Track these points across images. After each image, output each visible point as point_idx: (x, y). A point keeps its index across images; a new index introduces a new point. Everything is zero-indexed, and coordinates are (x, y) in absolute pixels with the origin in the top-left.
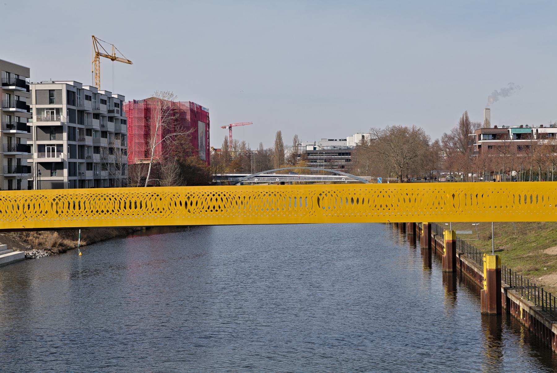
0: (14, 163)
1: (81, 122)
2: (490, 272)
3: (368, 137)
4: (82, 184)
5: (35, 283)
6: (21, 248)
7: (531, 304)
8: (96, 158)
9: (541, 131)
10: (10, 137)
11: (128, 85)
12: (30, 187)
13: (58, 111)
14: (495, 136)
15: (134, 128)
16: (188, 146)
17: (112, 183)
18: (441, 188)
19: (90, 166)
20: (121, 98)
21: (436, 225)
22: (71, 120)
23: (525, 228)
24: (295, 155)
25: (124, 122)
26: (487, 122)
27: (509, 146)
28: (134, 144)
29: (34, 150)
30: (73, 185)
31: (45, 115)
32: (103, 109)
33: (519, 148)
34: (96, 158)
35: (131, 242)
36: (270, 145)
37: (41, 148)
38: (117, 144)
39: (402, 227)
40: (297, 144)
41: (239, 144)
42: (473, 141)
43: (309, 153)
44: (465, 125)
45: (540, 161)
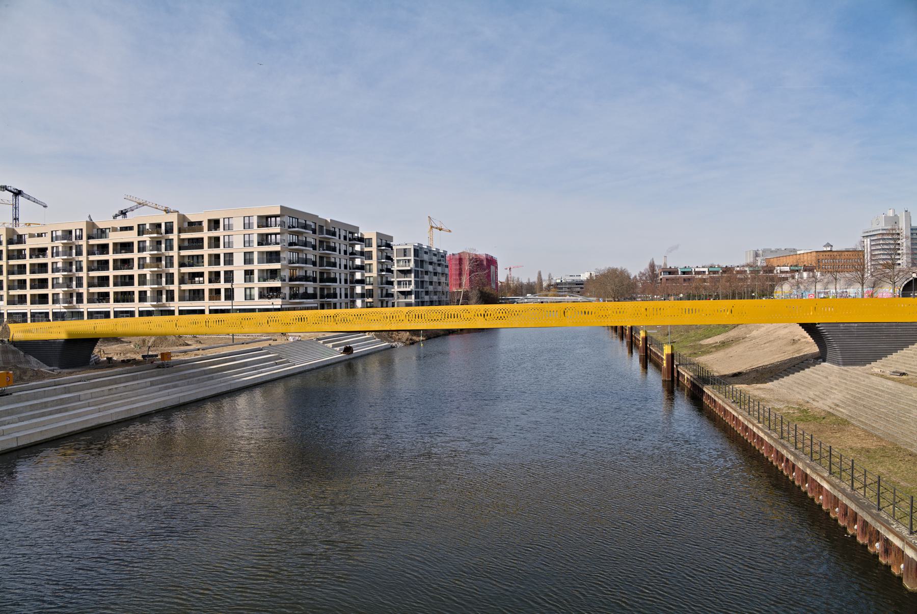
0: (384, 292)
1: (422, 267)
2: (667, 355)
3: (594, 274)
4: (423, 304)
5: (397, 360)
6: (389, 341)
7: (692, 374)
8: (431, 288)
9: (697, 270)
10: (382, 276)
11: (449, 245)
12: (393, 306)
13: (409, 261)
14: (670, 273)
15: (453, 270)
16: (485, 280)
17: (440, 303)
18: (638, 304)
19: (427, 293)
20: (445, 252)
21: (636, 327)
22: (416, 266)
23: (688, 328)
24: (549, 285)
25: (447, 266)
26: (665, 264)
27: (678, 279)
28: (453, 280)
29: (395, 284)
30: (417, 304)
31: (401, 263)
32: (435, 259)
33: (685, 280)
34: (431, 288)
35: (452, 339)
36: (534, 279)
37: (399, 283)
38: (443, 280)
39: (615, 329)
40: (550, 278)
41: (516, 278)
42: (657, 276)
43: (558, 284)
44: (652, 266)
45: (696, 288)
